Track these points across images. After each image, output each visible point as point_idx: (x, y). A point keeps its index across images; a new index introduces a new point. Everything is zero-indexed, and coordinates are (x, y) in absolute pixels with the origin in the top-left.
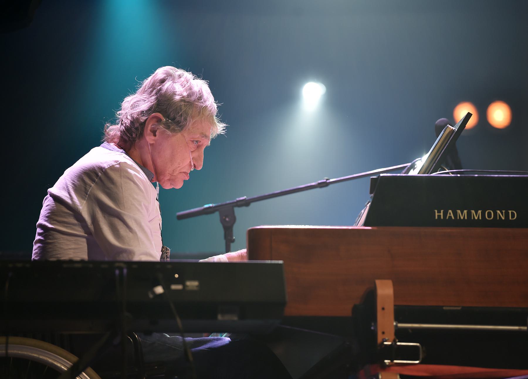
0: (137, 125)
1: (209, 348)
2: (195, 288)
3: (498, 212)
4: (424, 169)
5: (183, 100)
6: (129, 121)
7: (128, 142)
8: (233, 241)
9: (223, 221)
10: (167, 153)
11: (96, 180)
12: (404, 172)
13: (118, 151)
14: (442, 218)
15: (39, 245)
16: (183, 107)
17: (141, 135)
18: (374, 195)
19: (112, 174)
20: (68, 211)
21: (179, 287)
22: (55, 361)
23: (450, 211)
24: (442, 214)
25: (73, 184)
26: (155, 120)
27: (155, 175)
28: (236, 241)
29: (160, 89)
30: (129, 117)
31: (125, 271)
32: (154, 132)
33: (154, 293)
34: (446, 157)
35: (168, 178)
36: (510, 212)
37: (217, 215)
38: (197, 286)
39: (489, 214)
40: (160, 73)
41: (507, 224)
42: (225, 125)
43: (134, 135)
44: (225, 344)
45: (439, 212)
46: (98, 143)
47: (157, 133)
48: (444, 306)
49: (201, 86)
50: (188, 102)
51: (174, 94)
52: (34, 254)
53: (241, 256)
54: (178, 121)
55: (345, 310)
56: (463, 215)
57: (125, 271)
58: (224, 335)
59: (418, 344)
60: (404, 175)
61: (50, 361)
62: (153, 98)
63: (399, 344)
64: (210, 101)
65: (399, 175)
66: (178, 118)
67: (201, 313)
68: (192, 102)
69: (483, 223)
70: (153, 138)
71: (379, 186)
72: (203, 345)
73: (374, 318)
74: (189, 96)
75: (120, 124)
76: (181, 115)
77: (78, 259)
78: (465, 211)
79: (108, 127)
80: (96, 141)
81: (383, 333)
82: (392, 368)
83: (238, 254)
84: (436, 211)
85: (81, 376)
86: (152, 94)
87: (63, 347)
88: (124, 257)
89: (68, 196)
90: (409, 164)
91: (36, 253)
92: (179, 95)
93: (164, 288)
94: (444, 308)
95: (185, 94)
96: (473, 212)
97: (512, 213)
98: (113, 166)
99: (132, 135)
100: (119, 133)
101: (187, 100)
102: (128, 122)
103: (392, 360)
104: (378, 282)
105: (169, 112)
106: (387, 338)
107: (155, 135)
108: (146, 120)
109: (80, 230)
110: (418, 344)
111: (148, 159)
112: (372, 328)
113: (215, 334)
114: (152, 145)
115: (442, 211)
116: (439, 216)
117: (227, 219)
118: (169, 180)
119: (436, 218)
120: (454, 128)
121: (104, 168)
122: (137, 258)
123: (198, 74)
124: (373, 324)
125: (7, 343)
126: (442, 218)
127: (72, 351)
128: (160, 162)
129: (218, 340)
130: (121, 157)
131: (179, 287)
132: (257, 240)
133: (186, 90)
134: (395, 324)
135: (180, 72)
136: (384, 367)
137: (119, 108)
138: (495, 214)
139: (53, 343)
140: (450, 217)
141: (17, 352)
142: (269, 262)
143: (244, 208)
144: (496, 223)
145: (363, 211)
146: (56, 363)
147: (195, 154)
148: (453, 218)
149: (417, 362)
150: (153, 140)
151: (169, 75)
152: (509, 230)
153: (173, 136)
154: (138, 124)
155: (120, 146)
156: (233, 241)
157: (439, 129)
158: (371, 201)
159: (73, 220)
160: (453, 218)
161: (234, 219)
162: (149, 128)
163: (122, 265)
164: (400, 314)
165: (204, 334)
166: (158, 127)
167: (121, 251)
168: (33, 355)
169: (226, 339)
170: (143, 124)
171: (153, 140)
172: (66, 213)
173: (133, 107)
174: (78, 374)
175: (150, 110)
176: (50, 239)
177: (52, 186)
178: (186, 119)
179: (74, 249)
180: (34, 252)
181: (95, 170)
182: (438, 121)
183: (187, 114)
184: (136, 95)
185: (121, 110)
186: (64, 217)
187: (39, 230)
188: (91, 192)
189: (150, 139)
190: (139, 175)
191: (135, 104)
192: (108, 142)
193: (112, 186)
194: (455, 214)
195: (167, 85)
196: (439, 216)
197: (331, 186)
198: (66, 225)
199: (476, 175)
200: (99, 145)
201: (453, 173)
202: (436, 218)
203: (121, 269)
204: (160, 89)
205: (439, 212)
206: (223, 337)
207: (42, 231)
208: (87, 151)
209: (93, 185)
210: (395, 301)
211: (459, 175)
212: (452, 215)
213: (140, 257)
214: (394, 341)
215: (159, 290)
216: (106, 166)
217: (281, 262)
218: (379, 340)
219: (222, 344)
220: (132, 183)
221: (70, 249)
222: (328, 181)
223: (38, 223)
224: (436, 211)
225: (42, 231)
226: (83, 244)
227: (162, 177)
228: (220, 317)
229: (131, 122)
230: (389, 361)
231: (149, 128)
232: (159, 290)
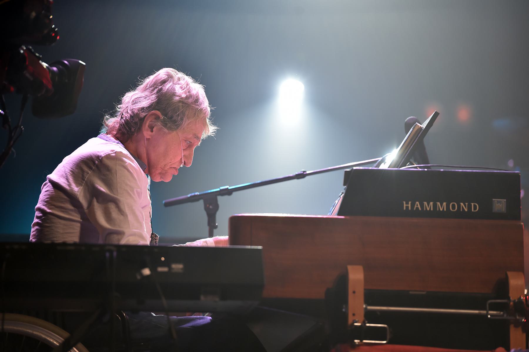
1: (192, 327)
3: (462, 204)
4: (393, 164)
6: (129, 115)
7: (126, 134)
8: (216, 227)
9: (207, 209)
10: (162, 149)
11: (94, 168)
12: (375, 165)
13: (114, 142)
14: (410, 209)
15: (37, 227)
16: (181, 108)
17: (140, 129)
18: (348, 187)
19: (108, 162)
20: (66, 197)
21: (165, 269)
22: (48, 336)
23: (418, 203)
24: (410, 205)
25: (71, 171)
26: (153, 117)
28: (219, 227)
29: (161, 89)
31: (115, 254)
32: (151, 128)
33: (141, 274)
34: (416, 150)
35: (160, 171)
37: (201, 203)
38: (182, 269)
40: (162, 73)
41: (469, 215)
43: (133, 130)
44: (207, 322)
45: (407, 203)
46: (95, 134)
47: (154, 129)
49: (198, 89)
50: (186, 103)
51: (174, 94)
52: (32, 236)
53: (225, 241)
54: (175, 120)
56: (429, 206)
57: (115, 254)
58: (207, 314)
59: (386, 326)
60: (375, 168)
61: (43, 336)
62: (154, 96)
63: (368, 325)
64: (205, 104)
65: (370, 168)
66: (175, 118)
67: (186, 292)
68: (190, 103)
69: (446, 214)
70: (150, 133)
71: (354, 180)
72: (186, 323)
73: (345, 301)
74: (187, 97)
75: (120, 118)
77: (72, 242)
78: (431, 203)
79: (107, 119)
80: (94, 132)
81: (354, 315)
82: (361, 347)
83: (221, 238)
84: (404, 202)
85: (72, 351)
86: (153, 93)
87: (55, 323)
88: (114, 239)
89: (66, 182)
90: (380, 159)
91: (34, 235)
92: (178, 96)
93: (151, 270)
94: (411, 292)
96: (439, 203)
98: (109, 154)
99: (131, 129)
100: (117, 126)
101: (186, 101)
102: (127, 116)
103: (361, 340)
104: (350, 268)
106: (357, 320)
107: (152, 131)
108: (146, 116)
109: (77, 215)
110: (386, 326)
111: (143, 151)
112: (344, 310)
113: (198, 313)
114: (148, 139)
115: (410, 203)
116: (407, 207)
117: (211, 207)
118: (160, 173)
119: (405, 208)
120: (422, 126)
121: (101, 156)
122: (124, 241)
123: (197, 79)
124: (344, 306)
125: (3, 320)
126: (410, 209)
128: (153, 156)
129: (200, 319)
130: (119, 148)
131: (165, 269)
132: (238, 225)
133: (185, 93)
134: (364, 306)
135: (180, 75)
137: (120, 102)
138: (459, 206)
139: (46, 319)
140: (417, 208)
142: (249, 247)
143: (226, 197)
144: (460, 214)
145: (337, 202)
146: (48, 339)
148: (420, 209)
149: (385, 342)
150: (150, 135)
151: (170, 77)
154: (138, 119)
155: (117, 138)
156: (216, 227)
157: (408, 126)
158: (344, 191)
159: (69, 206)
160: (420, 209)
161: (216, 207)
162: (147, 124)
164: (370, 297)
165: (187, 314)
166: (156, 124)
167: (111, 233)
168: (28, 331)
169: (208, 318)
170: (142, 120)
172: (65, 199)
173: (134, 102)
174: (70, 348)
175: (151, 107)
176: (47, 223)
177: (51, 173)
178: (182, 119)
179: (69, 233)
180: (32, 234)
182: (408, 119)
184: (136, 92)
185: (120, 104)
186: (62, 202)
187: (37, 214)
188: (88, 178)
189: (147, 134)
190: (132, 163)
191: (136, 99)
193: (108, 173)
194: (422, 205)
195: (168, 86)
196: (407, 207)
197: (307, 178)
198: (63, 210)
199: (442, 170)
200: (96, 136)
201: (420, 167)
202: (405, 208)
203: (111, 252)
204: (161, 89)
205: (407, 203)
206: (205, 316)
207: (41, 215)
208: (84, 141)
209: (90, 172)
211: (426, 170)
212: (419, 206)
213: (128, 240)
214: (364, 323)
215: (147, 272)
216: (102, 154)
217: (260, 247)
218: (350, 321)
219: (204, 323)
220: (126, 171)
221: (66, 233)
222: (305, 173)
223: (36, 207)
224: (404, 202)
225: (41, 215)
226: (76, 228)
228: (202, 298)
231: (147, 124)
232: (147, 272)
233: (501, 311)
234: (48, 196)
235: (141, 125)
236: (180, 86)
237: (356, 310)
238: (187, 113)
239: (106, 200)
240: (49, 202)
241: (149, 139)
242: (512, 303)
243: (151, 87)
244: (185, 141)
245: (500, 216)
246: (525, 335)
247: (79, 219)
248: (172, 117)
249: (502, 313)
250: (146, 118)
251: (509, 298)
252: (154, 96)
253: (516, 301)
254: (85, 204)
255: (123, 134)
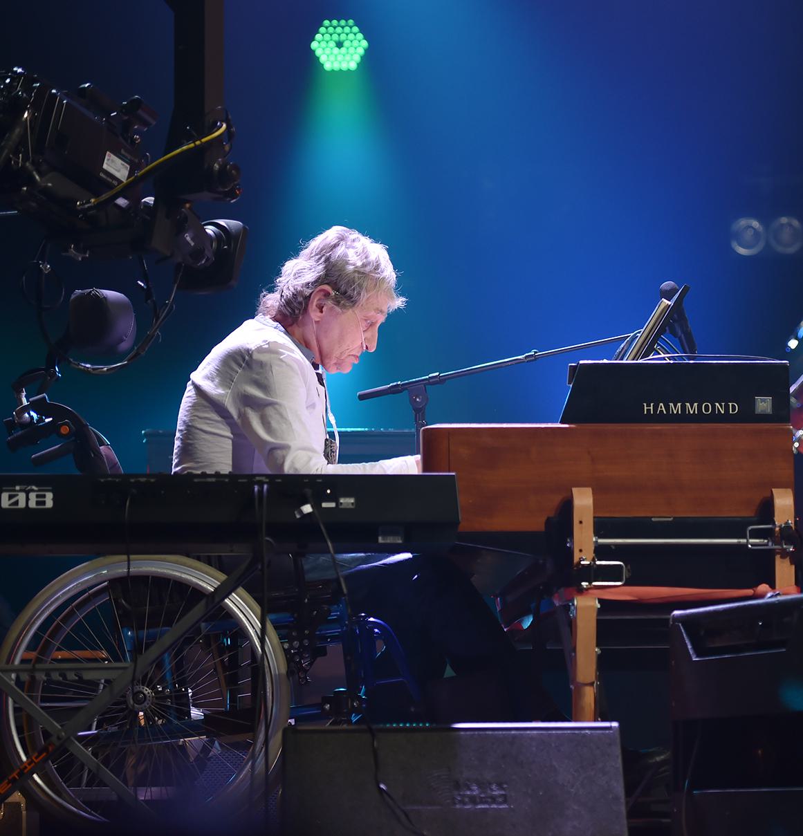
0: (300, 299)
2: (351, 506)
3: (717, 404)
5: (356, 271)
7: (292, 316)
10: (335, 333)
11: (243, 365)
21: (333, 505)
23: (662, 404)
26: (322, 293)
27: (318, 360)
30: (292, 289)
32: (321, 309)
33: (301, 512)
35: (335, 361)
36: (730, 404)
39: (707, 408)
40: (332, 234)
41: (727, 418)
42: (404, 299)
43: (297, 312)
45: (648, 405)
48: (652, 517)
49: (378, 253)
51: (347, 263)
55: (536, 523)
61: (195, 580)
62: (321, 267)
63: (598, 563)
64: (388, 272)
66: (349, 292)
67: (358, 534)
68: (367, 274)
70: (319, 314)
73: (570, 534)
74: (364, 265)
76: (354, 289)
78: (679, 404)
81: (581, 551)
82: (590, 591)
86: (321, 262)
94: (653, 519)
95: (359, 264)
97: (733, 406)
101: (362, 270)
102: (287, 293)
103: (590, 583)
104: (575, 490)
105: (338, 284)
107: (322, 312)
108: (311, 294)
109: (223, 427)
114: (317, 322)
116: (649, 411)
118: (335, 364)
124: (568, 540)
125: (129, 561)
127: (221, 569)
128: (325, 344)
131: (333, 505)
134: (594, 539)
135: (355, 235)
136: (581, 591)
137: (279, 274)
138: (714, 407)
140: (662, 411)
141: (156, 570)
146: (201, 583)
147: (368, 334)
148: (665, 412)
150: (319, 317)
151: (342, 239)
152: (728, 426)
153: (343, 313)
154: (302, 298)
155: (275, 319)
160: (665, 412)
162: (315, 304)
163: (264, 479)
164: (602, 527)
171: (319, 317)
173: (298, 275)
175: (318, 281)
178: (359, 294)
181: (241, 352)
183: (360, 286)
189: (314, 315)
191: (298, 272)
192: (264, 314)
194: (667, 407)
195: (340, 251)
196: (649, 411)
198: (208, 421)
200: (252, 316)
203: (261, 484)
205: (648, 405)
209: (239, 371)
210: (594, 512)
212: (663, 409)
214: (594, 560)
215: (307, 509)
216: (252, 346)
217: (454, 474)
218: (576, 560)
227: (326, 361)
228: (381, 540)
229: (293, 294)
230: (587, 584)
231: (315, 304)
232: (307, 509)
233: (765, 539)
234: (190, 405)
235: (307, 305)
236: (355, 250)
237: (584, 544)
238: (365, 285)
239: (260, 406)
240: (194, 407)
241: (318, 322)
242: (777, 529)
243: (317, 255)
244: (366, 320)
245: (764, 418)
246: (793, 567)
247: (229, 434)
248: (346, 292)
249: (766, 541)
250: (312, 295)
251: (774, 523)
252: (313, 274)
253: (783, 525)
254: (234, 412)
255: (284, 315)
